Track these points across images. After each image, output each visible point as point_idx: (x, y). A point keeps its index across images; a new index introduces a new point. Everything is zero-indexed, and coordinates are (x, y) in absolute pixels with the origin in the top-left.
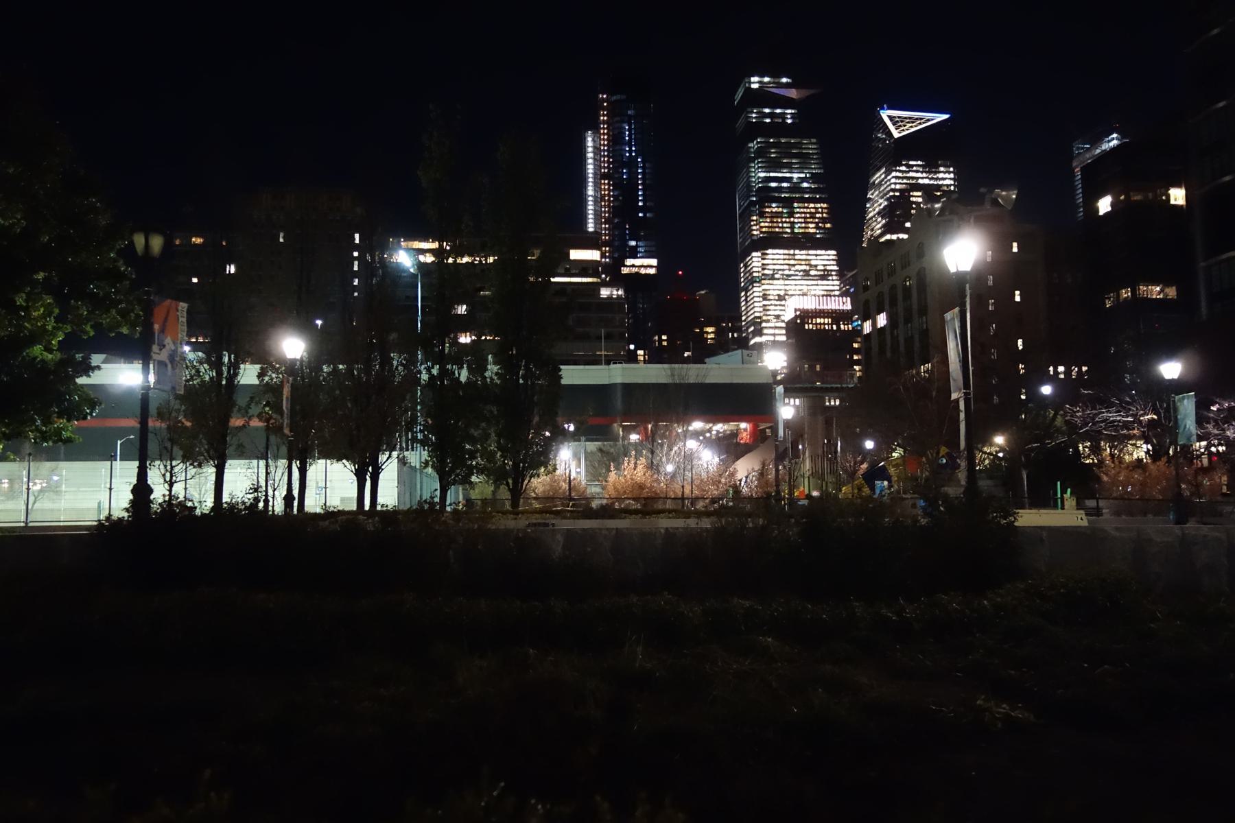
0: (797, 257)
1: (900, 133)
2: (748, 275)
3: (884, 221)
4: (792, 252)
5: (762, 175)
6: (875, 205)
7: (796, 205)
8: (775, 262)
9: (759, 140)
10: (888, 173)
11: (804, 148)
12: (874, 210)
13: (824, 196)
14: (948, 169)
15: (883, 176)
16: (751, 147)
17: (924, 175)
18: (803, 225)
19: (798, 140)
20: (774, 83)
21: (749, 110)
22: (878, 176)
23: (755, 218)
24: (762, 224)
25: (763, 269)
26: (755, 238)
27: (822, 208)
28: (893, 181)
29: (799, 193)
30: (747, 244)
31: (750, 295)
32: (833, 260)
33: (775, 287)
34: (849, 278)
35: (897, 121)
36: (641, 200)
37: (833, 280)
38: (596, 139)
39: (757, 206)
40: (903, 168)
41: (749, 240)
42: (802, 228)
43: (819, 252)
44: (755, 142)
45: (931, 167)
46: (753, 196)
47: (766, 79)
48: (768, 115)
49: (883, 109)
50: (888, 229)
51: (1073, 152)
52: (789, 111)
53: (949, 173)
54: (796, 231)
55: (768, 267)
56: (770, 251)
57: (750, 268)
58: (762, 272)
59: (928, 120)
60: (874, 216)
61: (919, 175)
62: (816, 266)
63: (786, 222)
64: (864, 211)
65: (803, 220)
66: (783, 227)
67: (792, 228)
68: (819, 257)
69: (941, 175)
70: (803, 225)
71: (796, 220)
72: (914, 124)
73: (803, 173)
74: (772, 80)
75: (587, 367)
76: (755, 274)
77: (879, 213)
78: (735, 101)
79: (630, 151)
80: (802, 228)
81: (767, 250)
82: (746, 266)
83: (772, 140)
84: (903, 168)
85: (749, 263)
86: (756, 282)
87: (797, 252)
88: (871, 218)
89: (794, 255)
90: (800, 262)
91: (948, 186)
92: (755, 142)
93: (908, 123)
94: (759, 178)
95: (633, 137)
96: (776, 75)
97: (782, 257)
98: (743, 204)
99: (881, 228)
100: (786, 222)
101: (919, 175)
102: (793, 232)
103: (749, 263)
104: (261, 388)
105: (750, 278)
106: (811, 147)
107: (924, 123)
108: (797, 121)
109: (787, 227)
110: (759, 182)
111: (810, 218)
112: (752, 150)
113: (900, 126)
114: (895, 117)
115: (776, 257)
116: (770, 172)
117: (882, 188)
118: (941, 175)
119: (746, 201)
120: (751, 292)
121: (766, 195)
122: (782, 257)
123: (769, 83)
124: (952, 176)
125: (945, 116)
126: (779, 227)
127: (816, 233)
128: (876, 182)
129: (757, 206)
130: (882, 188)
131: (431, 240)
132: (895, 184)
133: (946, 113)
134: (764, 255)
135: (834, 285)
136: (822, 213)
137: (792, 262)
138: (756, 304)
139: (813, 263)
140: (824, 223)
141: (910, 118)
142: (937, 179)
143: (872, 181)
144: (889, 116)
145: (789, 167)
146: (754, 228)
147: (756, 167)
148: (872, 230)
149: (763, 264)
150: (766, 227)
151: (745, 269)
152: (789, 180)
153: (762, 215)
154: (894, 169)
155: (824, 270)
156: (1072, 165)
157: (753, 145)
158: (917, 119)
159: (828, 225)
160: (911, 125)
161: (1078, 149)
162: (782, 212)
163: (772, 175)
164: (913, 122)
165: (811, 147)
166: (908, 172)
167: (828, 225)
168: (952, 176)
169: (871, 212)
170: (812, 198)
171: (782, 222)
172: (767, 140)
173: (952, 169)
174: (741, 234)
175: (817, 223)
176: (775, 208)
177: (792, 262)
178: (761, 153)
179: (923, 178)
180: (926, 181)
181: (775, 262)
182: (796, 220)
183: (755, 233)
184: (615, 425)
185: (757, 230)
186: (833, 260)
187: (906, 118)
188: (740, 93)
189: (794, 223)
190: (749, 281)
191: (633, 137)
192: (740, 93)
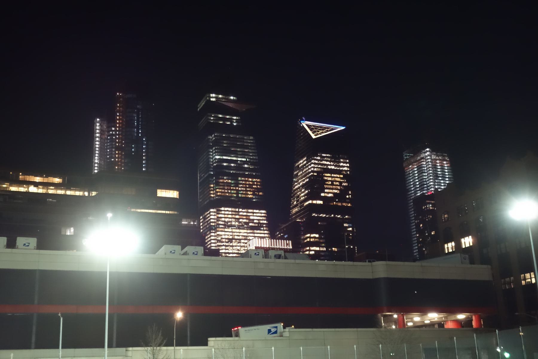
0: (241, 214)
1: (316, 136)
2: (206, 224)
3: (307, 191)
4: (237, 210)
5: (217, 157)
6: (300, 181)
7: (240, 178)
8: (226, 216)
10: (308, 160)
11: (246, 142)
12: (299, 184)
13: (257, 174)
14: (345, 161)
15: (305, 162)
16: (210, 139)
17: (332, 164)
18: (244, 192)
19: (241, 136)
20: (225, 99)
21: (209, 114)
22: (302, 162)
23: (212, 186)
24: (218, 190)
25: (218, 221)
26: (212, 199)
27: (256, 181)
28: (312, 165)
29: (241, 170)
30: (206, 203)
31: (208, 238)
32: (264, 216)
33: (225, 234)
34: (284, 228)
35: (313, 128)
36: (144, 167)
37: (264, 230)
38: (102, 124)
39: (214, 178)
40: (319, 158)
41: (208, 201)
42: (244, 194)
43: (255, 211)
44: (213, 136)
45: (335, 159)
46: (211, 171)
47: (220, 96)
48: (221, 119)
49: (303, 120)
50: (309, 197)
51: (403, 158)
52: (235, 118)
53: (347, 163)
54: (240, 195)
55: (221, 219)
56: (223, 209)
57: (208, 220)
58: (217, 223)
59: (333, 129)
60: (299, 188)
61: (328, 163)
62: (254, 220)
63: (233, 190)
64: (291, 184)
65: (244, 189)
66: (231, 193)
67: (237, 194)
68: (255, 214)
69: (341, 164)
70: (244, 192)
71: (240, 189)
72: (324, 131)
73: (245, 158)
74: (224, 97)
75: (356, 263)
76: (212, 224)
77: (303, 186)
78: (198, 108)
79: (138, 133)
80: (244, 194)
81: (221, 208)
82: (205, 218)
83: (224, 135)
84: (319, 158)
85: (207, 216)
86: (213, 229)
87: (240, 210)
88: (297, 189)
89: (239, 212)
90: (242, 217)
91: (346, 171)
92: (213, 136)
93: (320, 130)
94: (216, 159)
95: (140, 123)
96: (226, 94)
97: (230, 213)
98: (203, 176)
99: (304, 196)
100: (233, 190)
101: (328, 163)
102: (237, 197)
103: (207, 216)
104: (327, 253)
105: (208, 226)
106: (250, 140)
107: (330, 131)
108: (240, 124)
109: (234, 193)
110: (215, 163)
111: (248, 188)
112: (211, 140)
113: (315, 131)
114: (311, 126)
115: (226, 213)
116: (223, 156)
117: (305, 170)
118: (341, 164)
119: (206, 174)
120: (209, 236)
122: (230, 213)
123: (222, 98)
124: (348, 165)
125: (343, 128)
126: (228, 193)
127: (253, 198)
128: (300, 166)
129: (214, 178)
130: (305, 170)
131: (44, 176)
132: (314, 167)
133: (343, 126)
134: (219, 211)
135: (264, 234)
136: (257, 185)
137: (237, 217)
138: (212, 245)
139: (251, 218)
140: (259, 192)
141: (321, 127)
142: (339, 166)
143: (297, 164)
144: (307, 125)
145: (236, 154)
146: (212, 192)
147: (214, 152)
148: (298, 197)
149: (218, 217)
150: (220, 192)
151: (204, 220)
152: (235, 162)
153: (217, 184)
154: (313, 158)
155: (259, 223)
156: (403, 165)
157: (212, 137)
158: (325, 128)
159: (261, 193)
161: (406, 156)
162: (231, 183)
163: (224, 157)
165: (250, 140)
166: (322, 161)
167: (261, 193)
168: (348, 165)
169: (296, 185)
170: (251, 174)
171: (231, 190)
172: (221, 135)
173: (348, 161)
174: (201, 197)
175: (254, 192)
176: (226, 180)
177: (237, 217)
178: (217, 143)
179: (331, 165)
180: (333, 167)
181: (226, 216)
182: (240, 189)
183: (212, 195)
184: (379, 315)
185: (213, 194)
186: (264, 216)
187: (318, 127)
188: (202, 104)
189: (238, 190)
190: (207, 228)
191: (140, 123)
192: (202, 104)
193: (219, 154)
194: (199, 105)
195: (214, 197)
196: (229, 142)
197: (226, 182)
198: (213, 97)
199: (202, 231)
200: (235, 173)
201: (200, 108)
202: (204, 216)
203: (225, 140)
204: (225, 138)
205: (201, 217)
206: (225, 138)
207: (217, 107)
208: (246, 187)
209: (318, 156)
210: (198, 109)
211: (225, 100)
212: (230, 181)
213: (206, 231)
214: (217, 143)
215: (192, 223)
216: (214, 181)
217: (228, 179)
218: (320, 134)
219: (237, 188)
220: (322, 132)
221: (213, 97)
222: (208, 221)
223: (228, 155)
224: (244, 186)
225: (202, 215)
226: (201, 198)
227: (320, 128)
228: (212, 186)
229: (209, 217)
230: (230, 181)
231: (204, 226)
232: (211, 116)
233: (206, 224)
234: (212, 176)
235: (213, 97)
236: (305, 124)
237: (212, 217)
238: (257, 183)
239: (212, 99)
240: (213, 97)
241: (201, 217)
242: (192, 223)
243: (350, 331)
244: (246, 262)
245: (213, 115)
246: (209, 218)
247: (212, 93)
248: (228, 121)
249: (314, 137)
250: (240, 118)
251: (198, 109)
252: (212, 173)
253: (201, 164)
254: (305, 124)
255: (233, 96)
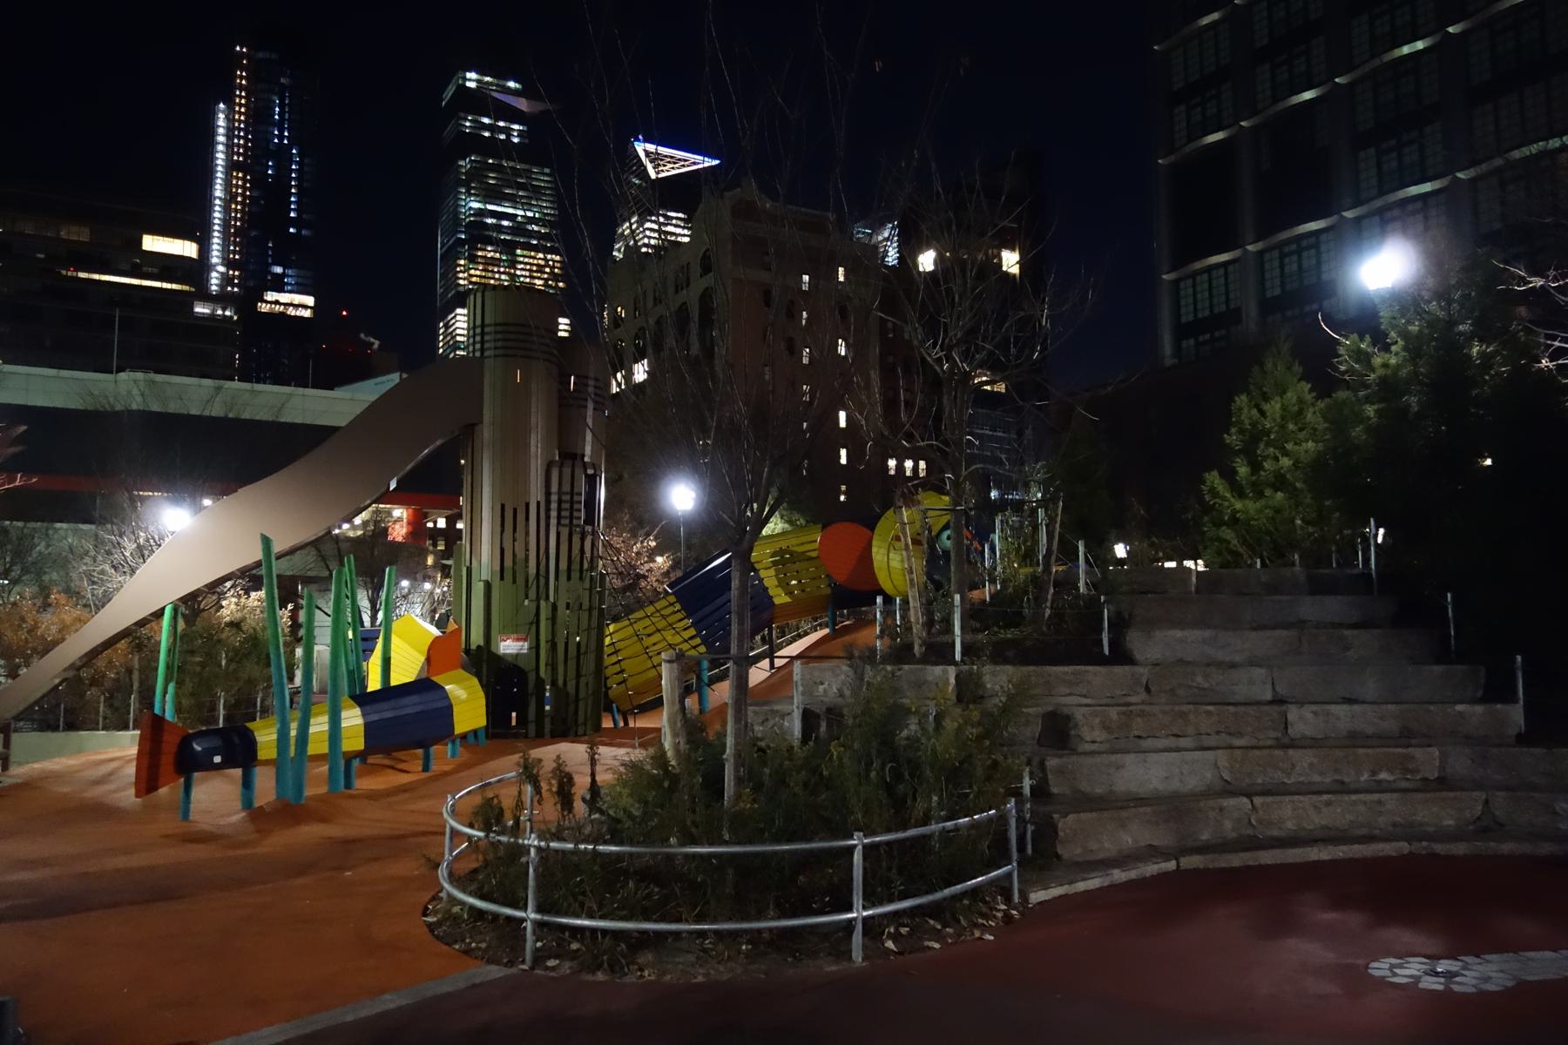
2: (449, 338)
7: (519, 252)
9: (473, 158)
20: (497, 85)
21: (462, 115)
23: (462, 262)
24: (472, 272)
26: (461, 289)
30: (450, 295)
39: (467, 247)
41: (453, 292)
44: (468, 160)
46: (461, 232)
47: (488, 79)
49: (639, 140)
52: (516, 127)
59: (694, 163)
61: (678, 231)
76: (458, 338)
78: (443, 100)
79: (281, 137)
82: (447, 326)
83: (491, 161)
92: (468, 160)
93: (669, 162)
94: (470, 208)
100: (504, 273)
101: (678, 231)
105: (451, 342)
106: (542, 177)
107: (688, 166)
108: (527, 141)
111: (536, 271)
121: (479, 233)
125: (716, 162)
129: (467, 247)
133: (715, 158)
141: (672, 157)
143: (620, 230)
145: (513, 200)
146: (461, 275)
150: (476, 276)
152: (512, 217)
153: (472, 259)
154: (649, 218)
158: (680, 160)
160: (672, 166)
161: (858, 232)
162: (500, 260)
164: (675, 163)
178: (477, 173)
183: (461, 282)
185: (464, 279)
187: (666, 156)
191: (287, 116)
193: (478, 199)
194: (444, 96)
195: (465, 285)
196: (499, 177)
197: (492, 258)
198: (470, 80)
199: (441, 351)
200: (509, 240)
201: (446, 100)
202: (445, 321)
203: (492, 171)
204: (492, 168)
205: (441, 324)
206: (492, 168)
207: (477, 102)
208: (530, 271)
209: (658, 215)
210: (443, 104)
211: (498, 89)
212: (498, 255)
213: (448, 351)
214: (477, 173)
215: (220, 312)
216: (466, 254)
217: (495, 251)
218: (668, 171)
219: (513, 271)
220: (683, 166)
221: (470, 80)
222: (452, 333)
223: (498, 202)
224: (528, 267)
225: (443, 320)
226: (443, 285)
227: (669, 160)
228: (462, 262)
229: (454, 324)
230: (498, 255)
231: (445, 341)
232: (466, 120)
233: (449, 338)
234: (461, 242)
235: (472, 79)
236: (640, 148)
237: (458, 325)
238: (554, 264)
239: (469, 84)
240: (472, 79)
241: (441, 324)
242: (220, 312)
243: (527, 550)
244: (334, 398)
245: (470, 118)
246: (454, 327)
247: (470, 71)
248: (502, 133)
249: (653, 175)
250: (528, 128)
251: (443, 104)
252: (463, 237)
253: (444, 218)
254: (640, 148)
255: (516, 82)
